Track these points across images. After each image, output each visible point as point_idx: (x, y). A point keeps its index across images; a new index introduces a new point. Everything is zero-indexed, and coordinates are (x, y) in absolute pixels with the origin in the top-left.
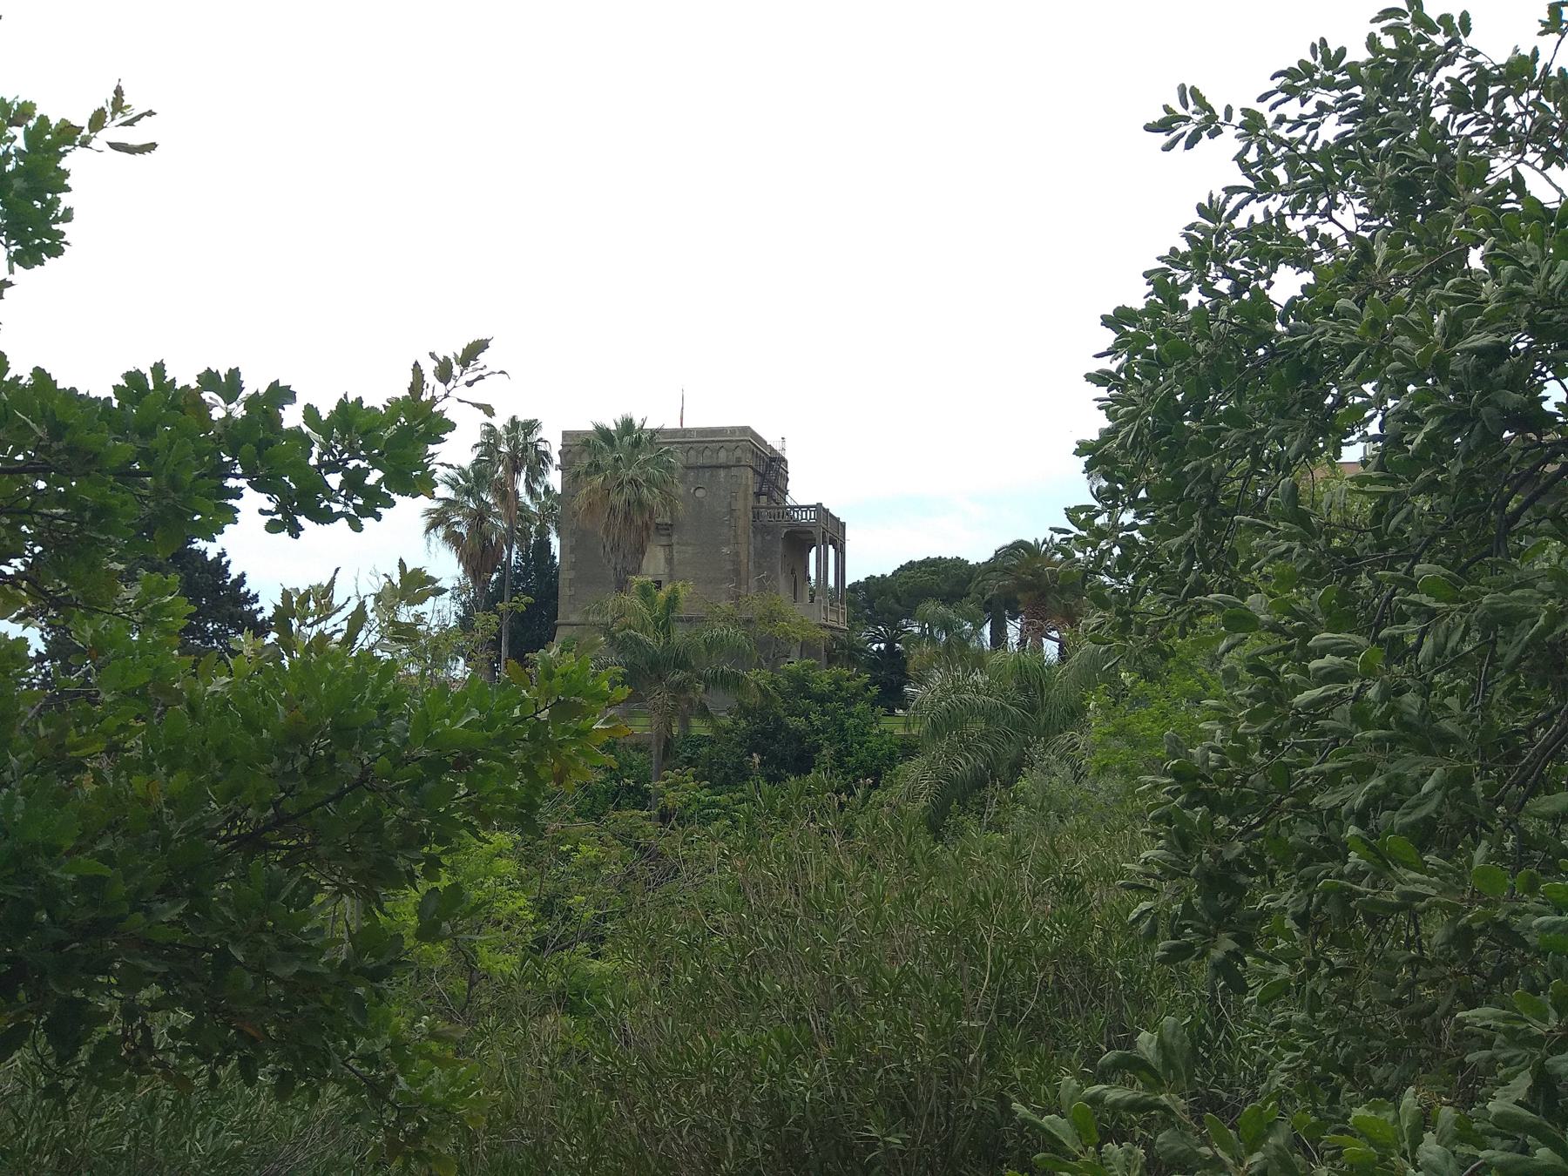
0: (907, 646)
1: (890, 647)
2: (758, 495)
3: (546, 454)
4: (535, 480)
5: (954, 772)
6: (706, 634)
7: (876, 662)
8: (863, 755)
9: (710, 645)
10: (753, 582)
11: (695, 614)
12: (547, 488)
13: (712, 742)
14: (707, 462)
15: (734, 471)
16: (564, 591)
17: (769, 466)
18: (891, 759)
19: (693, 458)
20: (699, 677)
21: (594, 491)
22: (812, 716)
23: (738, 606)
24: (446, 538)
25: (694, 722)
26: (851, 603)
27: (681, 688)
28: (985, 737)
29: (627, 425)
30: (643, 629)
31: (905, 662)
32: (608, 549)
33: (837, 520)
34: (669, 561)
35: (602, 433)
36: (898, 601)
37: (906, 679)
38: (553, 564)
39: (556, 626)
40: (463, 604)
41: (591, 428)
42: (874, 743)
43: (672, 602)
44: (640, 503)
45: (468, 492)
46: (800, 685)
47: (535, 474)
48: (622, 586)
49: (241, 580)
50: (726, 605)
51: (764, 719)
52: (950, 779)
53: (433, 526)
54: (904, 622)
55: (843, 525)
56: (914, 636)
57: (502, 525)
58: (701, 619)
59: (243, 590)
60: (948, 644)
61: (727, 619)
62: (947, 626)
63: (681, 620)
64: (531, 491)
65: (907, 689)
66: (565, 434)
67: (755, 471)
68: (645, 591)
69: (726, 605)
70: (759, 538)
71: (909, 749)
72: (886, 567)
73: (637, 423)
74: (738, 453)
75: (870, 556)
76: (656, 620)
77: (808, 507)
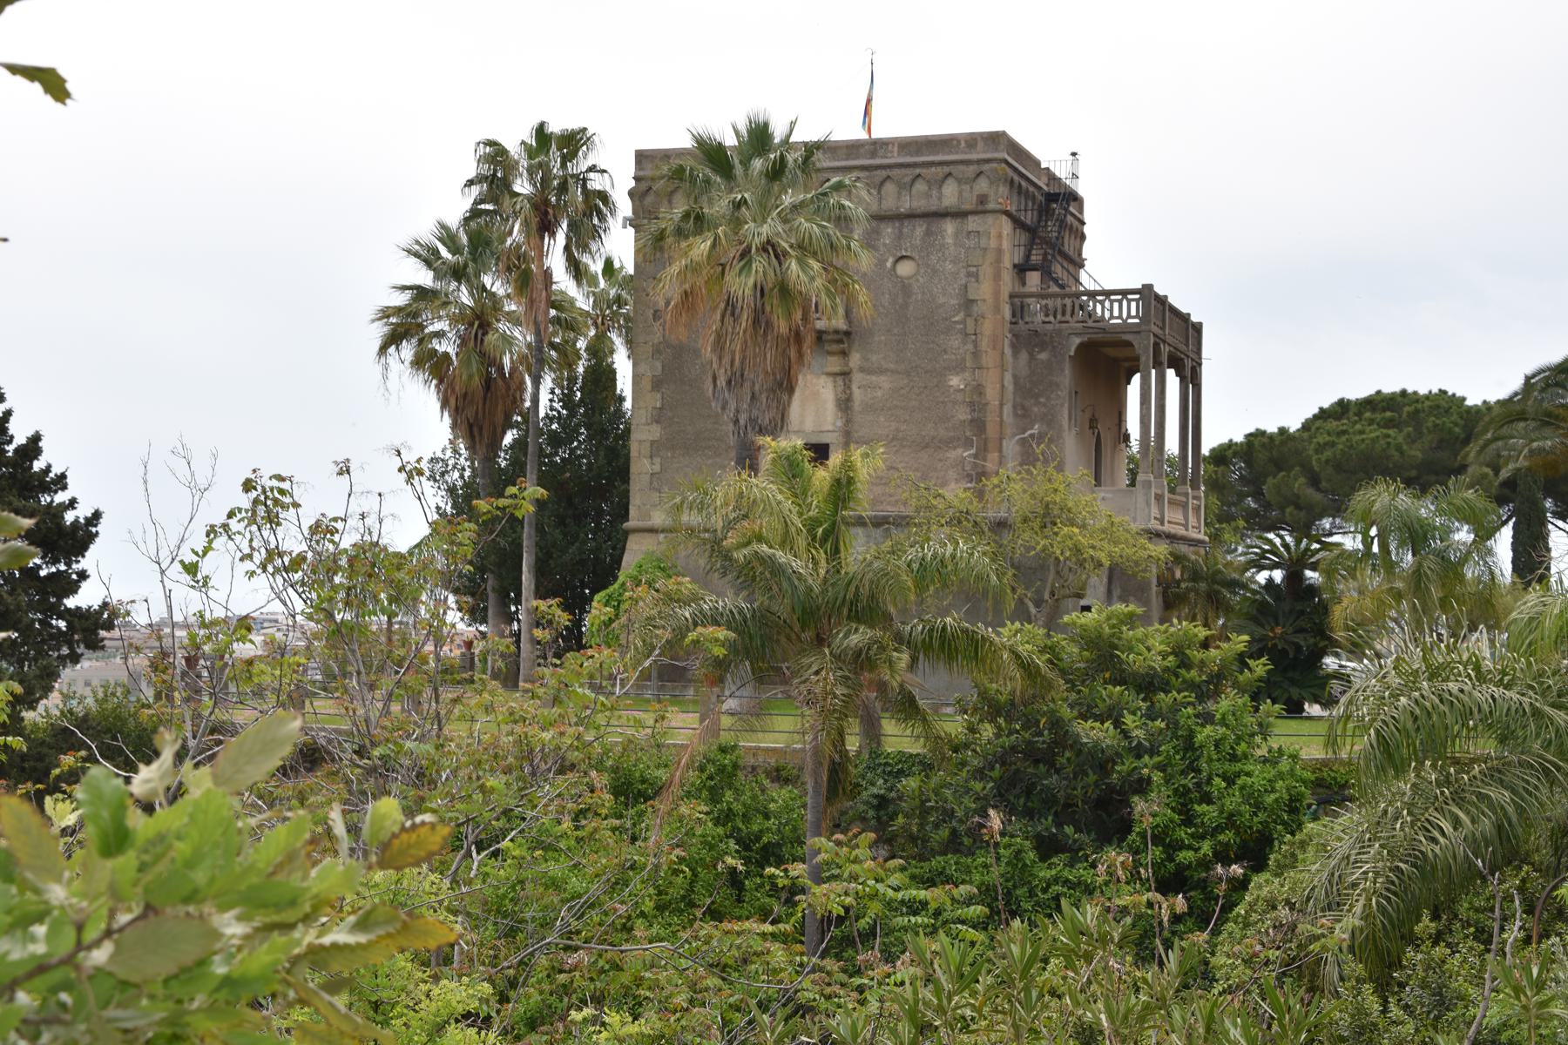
0: (1329, 573)
1: (1294, 577)
2: (1021, 269)
3: (603, 196)
4: (585, 248)
5: (1426, 847)
6: (912, 553)
7: (1266, 608)
8: (1233, 801)
9: (925, 573)
10: (1011, 447)
11: (890, 510)
12: (609, 264)
13: (927, 767)
14: (921, 204)
15: (973, 223)
16: (642, 466)
17: (1044, 211)
18: (1293, 810)
19: (892, 199)
20: (898, 638)
21: (693, 268)
22: (1129, 720)
23: (980, 494)
24: (418, 363)
25: (889, 726)
26: (1215, 486)
27: (861, 661)
28: (1496, 774)
29: (759, 136)
30: (786, 542)
31: (1324, 609)
32: (722, 382)
33: (1185, 318)
34: (845, 404)
35: (711, 152)
36: (1314, 481)
37: (1328, 644)
38: (619, 413)
39: (627, 533)
40: (451, 490)
41: (687, 143)
42: (1258, 776)
43: (842, 490)
44: (784, 290)
45: (458, 273)
46: (1104, 655)
47: (584, 234)
48: (748, 459)
49: (33, 447)
50: (956, 493)
51: (1030, 723)
52: (1422, 863)
53: (393, 339)
54: (1326, 523)
55: (1198, 328)
56: (1345, 554)
57: (522, 337)
58: (902, 522)
59: (38, 466)
60: (1418, 574)
61: (956, 521)
62: (1416, 536)
63: (860, 522)
64: (577, 270)
65: (1330, 662)
66: (642, 157)
67: (1018, 223)
68: (790, 470)
69: (956, 493)
70: (1024, 356)
71: (1330, 791)
72: (1288, 412)
73: (778, 131)
74: (983, 185)
75: (1252, 392)
76: (811, 525)
77: (1124, 293)
